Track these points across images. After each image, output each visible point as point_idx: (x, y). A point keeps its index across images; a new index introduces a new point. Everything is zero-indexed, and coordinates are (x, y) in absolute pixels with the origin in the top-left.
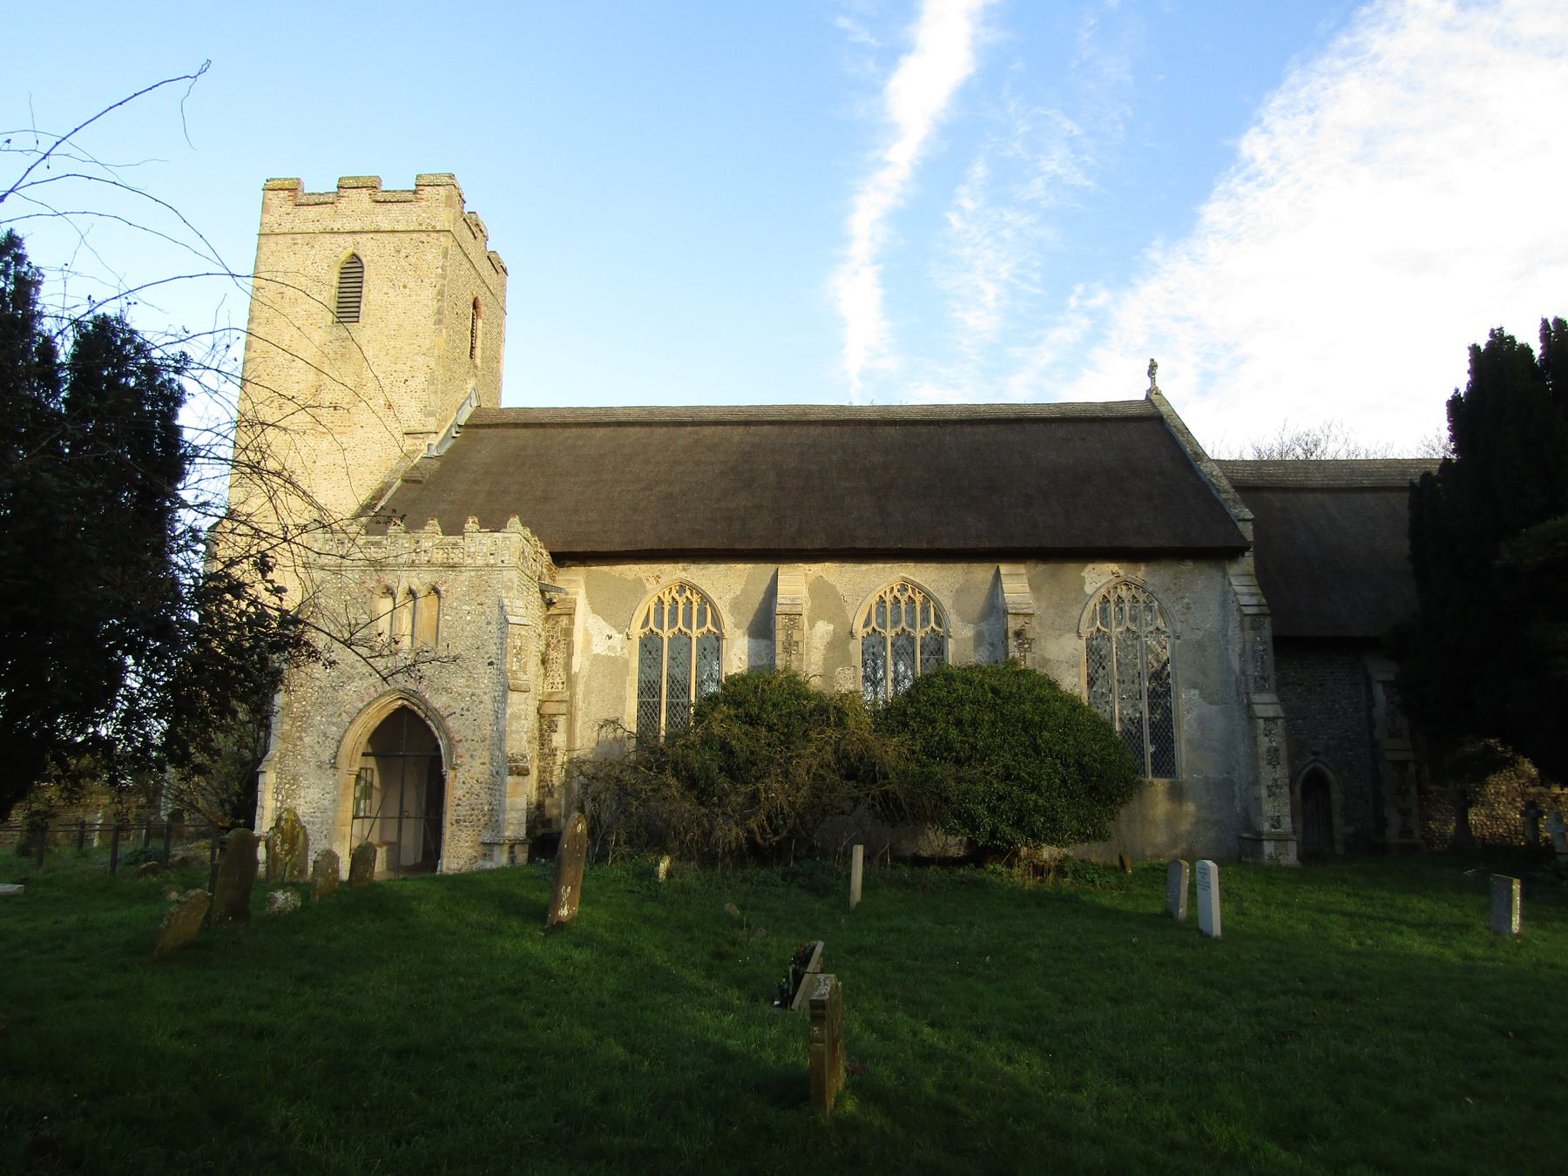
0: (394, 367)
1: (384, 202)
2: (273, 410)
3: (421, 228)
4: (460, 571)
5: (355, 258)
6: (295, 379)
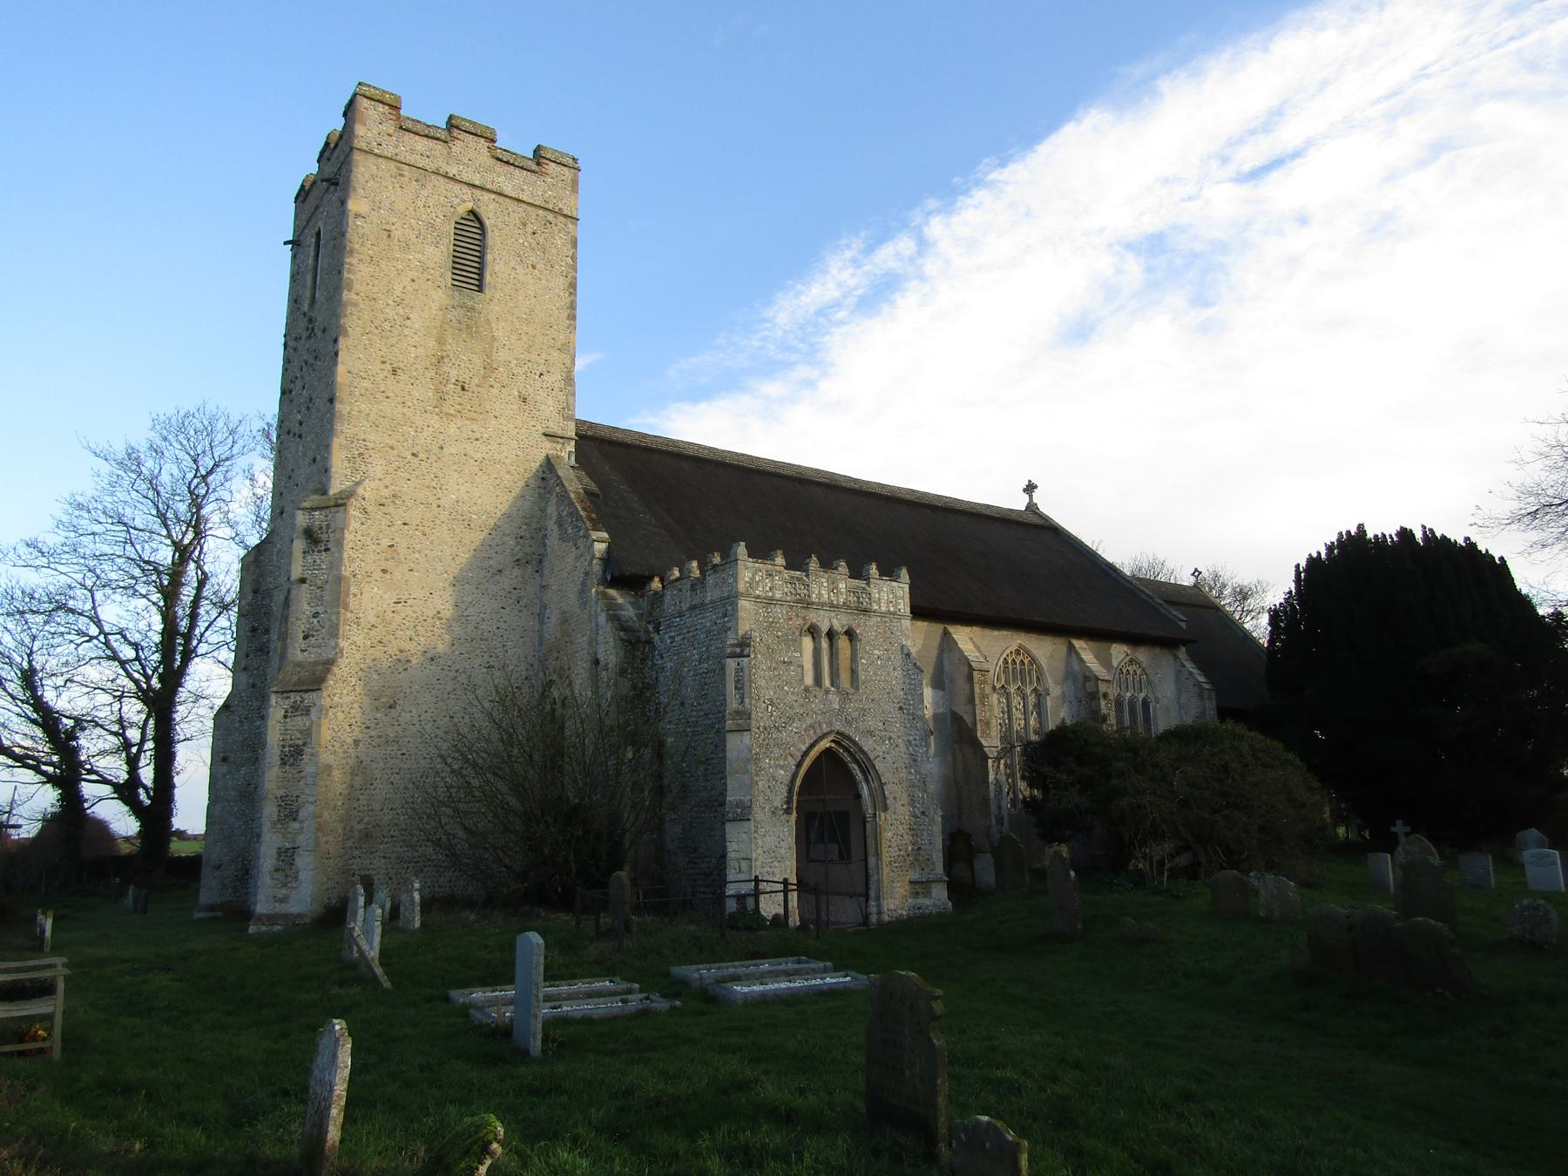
0: (526, 356)
1: (507, 163)
2: (385, 373)
3: (547, 206)
4: (870, 616)
5: (474, 215)
6: (412, 342)
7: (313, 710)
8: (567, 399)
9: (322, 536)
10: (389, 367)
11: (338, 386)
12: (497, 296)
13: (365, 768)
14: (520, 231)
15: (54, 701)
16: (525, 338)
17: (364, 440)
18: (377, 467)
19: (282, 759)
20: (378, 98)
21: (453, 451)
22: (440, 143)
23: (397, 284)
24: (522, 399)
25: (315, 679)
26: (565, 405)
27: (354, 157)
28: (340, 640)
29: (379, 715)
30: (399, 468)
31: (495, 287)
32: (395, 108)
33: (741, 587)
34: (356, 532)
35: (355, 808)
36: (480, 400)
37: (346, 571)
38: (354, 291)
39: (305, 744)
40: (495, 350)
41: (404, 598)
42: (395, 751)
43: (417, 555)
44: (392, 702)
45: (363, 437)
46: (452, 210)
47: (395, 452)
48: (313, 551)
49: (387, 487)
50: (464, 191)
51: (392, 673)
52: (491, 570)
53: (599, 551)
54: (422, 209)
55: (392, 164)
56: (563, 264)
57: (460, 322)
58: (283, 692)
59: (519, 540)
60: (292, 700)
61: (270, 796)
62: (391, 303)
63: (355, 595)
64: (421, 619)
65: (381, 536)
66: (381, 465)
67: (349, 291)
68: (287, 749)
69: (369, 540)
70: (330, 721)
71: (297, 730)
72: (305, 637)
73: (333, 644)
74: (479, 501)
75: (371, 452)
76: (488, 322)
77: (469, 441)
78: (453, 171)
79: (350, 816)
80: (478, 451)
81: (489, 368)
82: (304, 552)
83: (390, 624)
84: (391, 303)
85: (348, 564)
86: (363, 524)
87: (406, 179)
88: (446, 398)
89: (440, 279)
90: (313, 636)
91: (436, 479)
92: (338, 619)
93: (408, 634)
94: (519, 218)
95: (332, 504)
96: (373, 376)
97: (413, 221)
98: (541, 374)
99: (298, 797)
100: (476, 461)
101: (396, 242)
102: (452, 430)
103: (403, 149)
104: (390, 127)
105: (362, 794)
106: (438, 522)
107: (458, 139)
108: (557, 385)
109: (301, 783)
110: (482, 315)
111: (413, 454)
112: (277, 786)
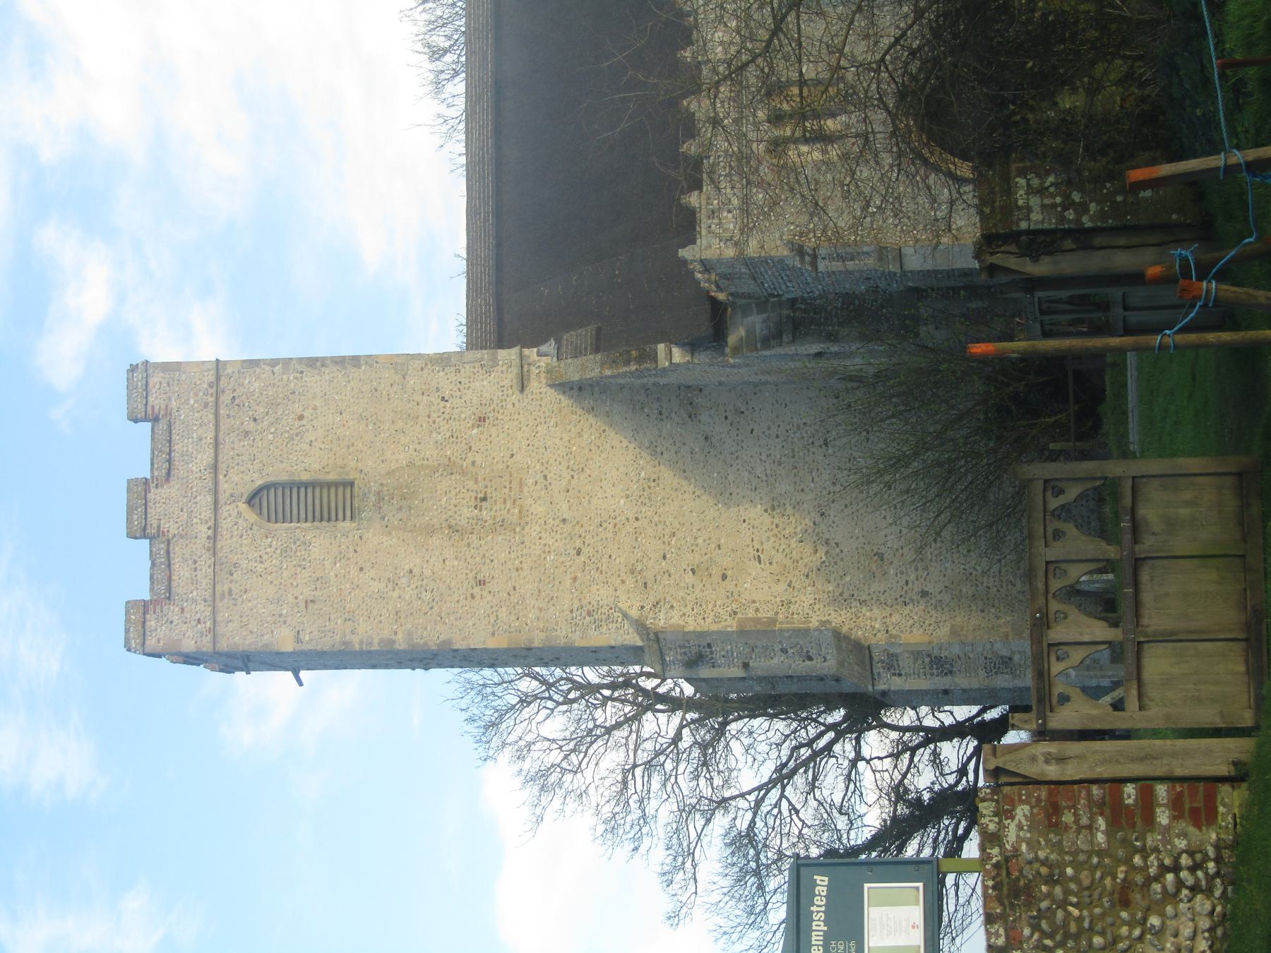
5: (254, 499)
7: (892, 651)
8: (468, 363)
9: (693, 652)
10: (477, 590)
11: (513, 646)
12: (353, 464)
13: (952, 583)
14: (258, 438)
15: (873, 829)
16: (400, 424)
17: (572, 611)
18: (601, 595)
19: (946, 674)
20: (140, 628)
21: (565, 506)
22: (171, 549)
23: (371, 589)
24: (482, 423)
25: (860, 651)
26: (477, 365)
27: (226, 649)
28: (811, 625)
29: (892, 571)
30: (598, 569)
31: (343, 467)
32: (145, 606)
33: (730, 252)
34: (684, 614)
35: (998, 591)
36: (495, 477)
37: (731, 625)
38: (393, 637)
39: (929, 656)
40: (425, 462)
41: (752, 553)
42: (932, 550)
43: (700, 541)
44: (876, 558)
45: (567, 612)
46: (255, 528)
47: (579, 575)
48: (712, 658)
49: (623, 582)
50: (225, 514)
51: (842, 560)
52: (706, 450)
53: (684, 356)
54: (267, 565)
55: (219, 604)
56: (285, 378)
57: (400, 508)
58: (873, 679)
59: (664, 417)
60: (882, 670)
61: (986, 683)
62: (396, 594)
63: (757, 610)
64: (775, 531)
65: (682, 585)
66: (598, 590)
67: (394, 642)
68: (935, 671)
69: (689, 598)
70: (902, 631)
71: (915, 663)
72: (810, 659)
73: (816, 633)
74: (622, 469)
75: (584, 602)
76: (390, 473)
77: (549, 488)
78: (204, 531)
79: (1006, 595)
80: (560, 476)
81: (450, 468)
82: (713, 667)
83: (785, 566)
84: (396, 594)
85: (723, 624)
86: (672, 607)
87: (233, 586)
88: (500, 519)
89: (350, 535)
90: (808, 652)
91: (604, 524)
92: (787, 630)
93: (795, 545)
94: (240, 440)
95: (656, 646)
96: (492, 607)
97: (285, 575)
98: (443, 399)
99: (986, 658)
100: (572, 477)
101: (318, 593)
102: (539, 509)
103: (195, 593)
104: (172, 611)
105: (982, 583)
106: (656, 518)
107: (159, 527)
108: (453, 377)
109: (971, 656)
110: (384, 482)
111: (578, 554)
112: (975, 677)
